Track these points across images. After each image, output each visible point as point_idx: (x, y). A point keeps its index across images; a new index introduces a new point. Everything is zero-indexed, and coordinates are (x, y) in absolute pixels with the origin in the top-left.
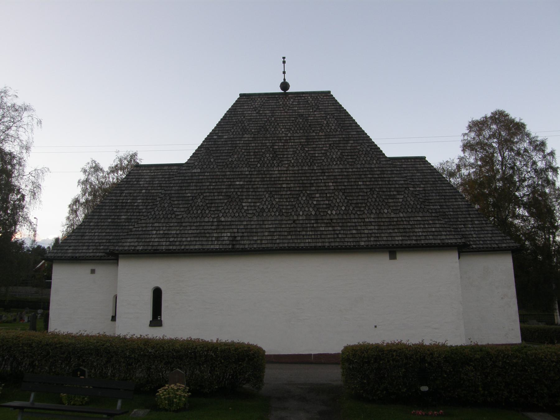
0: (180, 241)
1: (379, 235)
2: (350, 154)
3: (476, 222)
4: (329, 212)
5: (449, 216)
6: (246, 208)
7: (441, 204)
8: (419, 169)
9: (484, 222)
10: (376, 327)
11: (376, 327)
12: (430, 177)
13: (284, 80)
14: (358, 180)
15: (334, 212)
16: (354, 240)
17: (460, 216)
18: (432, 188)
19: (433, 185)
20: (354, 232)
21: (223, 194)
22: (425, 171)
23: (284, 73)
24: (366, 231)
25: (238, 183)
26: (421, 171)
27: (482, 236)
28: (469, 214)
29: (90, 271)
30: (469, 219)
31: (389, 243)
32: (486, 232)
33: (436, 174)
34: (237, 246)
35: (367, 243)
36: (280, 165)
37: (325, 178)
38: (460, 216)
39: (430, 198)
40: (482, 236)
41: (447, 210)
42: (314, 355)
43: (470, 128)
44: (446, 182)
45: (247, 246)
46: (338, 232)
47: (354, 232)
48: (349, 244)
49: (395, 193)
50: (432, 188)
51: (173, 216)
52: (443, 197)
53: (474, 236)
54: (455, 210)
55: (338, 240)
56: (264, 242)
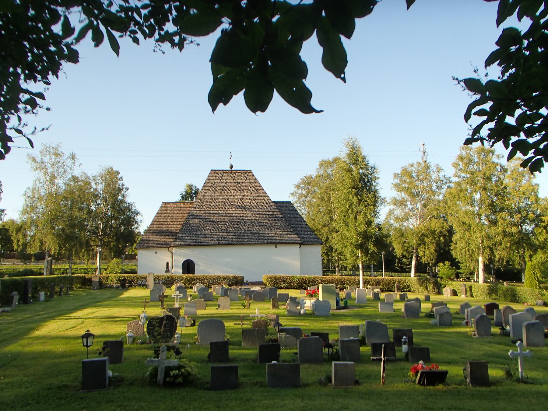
43: (321, 165)
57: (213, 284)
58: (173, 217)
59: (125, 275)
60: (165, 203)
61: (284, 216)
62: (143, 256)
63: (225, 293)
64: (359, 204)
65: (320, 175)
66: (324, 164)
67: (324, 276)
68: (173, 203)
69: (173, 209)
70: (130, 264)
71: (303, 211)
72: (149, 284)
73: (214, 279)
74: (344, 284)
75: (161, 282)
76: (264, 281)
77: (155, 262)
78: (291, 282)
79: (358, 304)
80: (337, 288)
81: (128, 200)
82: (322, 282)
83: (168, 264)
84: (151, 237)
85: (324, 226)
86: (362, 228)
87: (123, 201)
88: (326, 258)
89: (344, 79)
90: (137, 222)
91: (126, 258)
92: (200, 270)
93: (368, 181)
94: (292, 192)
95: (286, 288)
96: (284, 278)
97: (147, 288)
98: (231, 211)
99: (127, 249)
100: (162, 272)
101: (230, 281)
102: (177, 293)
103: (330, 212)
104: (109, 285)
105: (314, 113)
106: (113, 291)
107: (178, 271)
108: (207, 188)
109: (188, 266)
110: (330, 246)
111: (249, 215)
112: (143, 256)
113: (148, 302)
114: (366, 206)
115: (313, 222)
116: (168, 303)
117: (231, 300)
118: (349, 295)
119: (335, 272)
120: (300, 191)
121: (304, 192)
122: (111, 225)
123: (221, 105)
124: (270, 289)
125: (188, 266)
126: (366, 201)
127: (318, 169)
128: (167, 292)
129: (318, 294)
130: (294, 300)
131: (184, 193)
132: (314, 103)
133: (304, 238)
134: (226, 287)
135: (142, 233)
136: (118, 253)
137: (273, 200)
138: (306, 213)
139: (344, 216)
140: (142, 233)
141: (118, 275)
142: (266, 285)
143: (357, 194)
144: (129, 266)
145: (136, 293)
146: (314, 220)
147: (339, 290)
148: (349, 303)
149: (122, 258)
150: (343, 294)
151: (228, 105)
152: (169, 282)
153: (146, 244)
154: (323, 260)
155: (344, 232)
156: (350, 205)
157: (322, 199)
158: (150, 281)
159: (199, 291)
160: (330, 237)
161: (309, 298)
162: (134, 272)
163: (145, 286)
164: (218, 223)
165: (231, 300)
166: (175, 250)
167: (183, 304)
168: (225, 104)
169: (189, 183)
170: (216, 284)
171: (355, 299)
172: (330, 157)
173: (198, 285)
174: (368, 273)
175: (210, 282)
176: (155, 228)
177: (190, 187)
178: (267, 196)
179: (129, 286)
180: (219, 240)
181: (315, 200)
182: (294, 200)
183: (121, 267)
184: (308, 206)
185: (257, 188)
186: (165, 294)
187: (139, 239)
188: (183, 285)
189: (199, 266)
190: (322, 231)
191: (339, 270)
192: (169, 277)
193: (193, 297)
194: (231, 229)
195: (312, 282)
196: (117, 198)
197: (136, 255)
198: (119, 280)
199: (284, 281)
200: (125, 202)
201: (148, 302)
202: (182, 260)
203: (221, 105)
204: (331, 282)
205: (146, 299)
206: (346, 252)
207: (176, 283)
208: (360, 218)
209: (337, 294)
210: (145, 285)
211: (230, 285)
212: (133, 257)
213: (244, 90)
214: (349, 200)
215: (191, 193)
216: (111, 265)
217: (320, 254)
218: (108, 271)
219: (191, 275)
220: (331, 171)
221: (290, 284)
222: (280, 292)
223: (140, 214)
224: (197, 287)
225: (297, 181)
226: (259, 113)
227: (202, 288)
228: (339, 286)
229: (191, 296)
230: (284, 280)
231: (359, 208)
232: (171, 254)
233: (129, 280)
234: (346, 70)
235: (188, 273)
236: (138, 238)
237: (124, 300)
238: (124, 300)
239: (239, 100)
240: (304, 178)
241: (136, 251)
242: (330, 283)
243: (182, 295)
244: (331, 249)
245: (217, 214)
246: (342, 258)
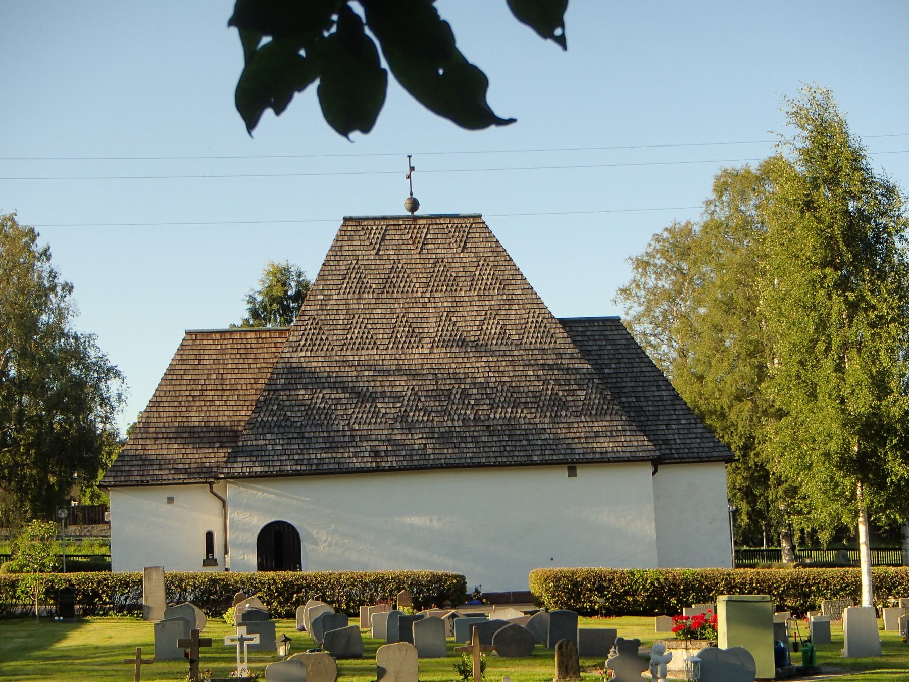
0: (308, 459)
1: (555, 447)
2: (515, 327)
3: (683, 422)
4: (492, 416)
5: (648, 413)
6: (383, 411)
7: (638, 394)
8: (610, 338)
9: (693, 421)
12: (625, 351)
13: (411, 194)
14: (526, 368)
16: (526, 453)
17: (662, 413)
18: (626, 370)
19: (628, 365)
20: (525, 442)
21: (350, 391)
22: (618, 342)
24: (540, 442)
26: (612, 342)
27: (688, 441)
28: (675, 410)
30: (674, 417)
31: (568, 457)
32: (693, 436)
33: (633, 346)
34: (383, 464)
35: (541, 458)
38: (662, 413)
39: (623, 385)
40: (688, 441)
41: (645, 404)
43: (721, 188)
44: (647, 360)
45: (395, 464)
46: (504, 443)
47: (525, 442)
48: (519, 459)
49: (575, 387)
50: (626, 370)
51: (289, 423)
52: (641, 384)
53: (678, 441)
54: (656, 403)
55: (506, 454)
57: (362, 603)
58: (222, 381)
59: (72, 575)
60: (194, 336)
61: (599, 368)
62: (123, 507)
63: (402, 630)
64: (851, 318)
65: (719, 225)
66: (732, 184)
67: (742, 570)
68: (222, 333)
69: (222, 352)
70: (86, 541)
71: (663, 351)
72: (150, 604)
73: (366, 584)
74: (807, 595)
75: (190, 597)
76: (535, 588)
77: (166, 532)
78: (626, 593)
79: (851, 660)
80: (780, 609)
81: (75, 325)
82: (730, 588)
83: (209, 536)
84: (152, 451)
85: (738, 398)
86: (861, 403)
87: (55, 331)
88: (745, 507)
89: (562, 41)
90: (104, 401)
91: (73, 519)
92: (320, 557)
93: (877, 237)
94: (626, 282)
95: (609, 613)
96: (600, 577)
97: (145, 619)
98: (415, 357)
99: (76, 491)
100: (189, 563)
101: (420, 591)
102: (242, 631)
103: (756, 350)
104: (19, 610)
105: (493, 128)
106: (31, 627)
107: (243, 560)
108: (334, 280)
109: (279, 545)
110: (761, 467)
111: (477, 368)
112: (123, 507)
113: (148, 662)
114: (872, 325)
115: (697, 386)
116: (210, 665)
117: (420, 656)
118: (821, 629)
119: (776, 555)
120: (651, 281)
121: (665, 283)
122: (21, 413)
123: (269, 113)
124: (553, 615)
125: (279, 545)
126: (874, 308)
127: (709, 203)
128: (210, 629)
129: (715, 629)
130: (630, 648)
131: (259, 298)
132: (497, 100)
133: (666, 442)
134: (406, 610)
135: (123, 435)
136: (48, 504)
137: (558, 315)
138: (674, 354)
139: (801, 363)
140: (123, 435)
141: (49, 576)
142: (540, 604)
143: (843, 285)
144: (85, 547)
145: (110, 633)
146: (701, 378)
147: (788, 614)
148: (822, 655)
149: (59, 520)
150: (801, 630)
151: (284, 114)
152: (216, 597)
153: (139, 471)
154: (735, 514)
155: (802, 418)
156: (822, 325)
157: (729, 306)
158: (154, 596)
159: (315, 624)
160: (758, 434)
161: (683, 644)
162: (100, 564)
163: (135, 610)
164: (373, 398)
165: (420, 656)
166: (232, 491)
167: (263, 669)
168: (278, 112)
169: (281, 261)
170: (372, 602)
171: (840, 644)
172: (751, 158)
173: (311, 604)
174: (892, 556)
175: (349, 596)
176: (165, 416)
177: (281, 275)
178: (538, 302)
179: (86, 613)
180: (377, 453)
181: (702, 311)
182: (632, 312)
183: (56, 549)
184: (678, 331)
185: (502, 275)
186: (203, 635)
187: (114, 457)
188: (264, 607)
189: (315, 542)
190: (732, 417)
191: (793, 548)
192: (214, 581)
193: (295, 646)
194: (421, 417)
195: (698, 590)
196: (35, 320)
197: (104, 508)
198: (48, 592)
199: (601, 590)
200: (63, 334)
201: (148, 662)
202: (260, 522)
203: (269, 113)
204: (764, 587)
205: (139, 652)
206: (812, 487)
207: (239, 600)
208: (854, 364)
209: (780, 629)
210: (140, 607)
211: (418, 606)
212: (95, 516)
213: (317, 82)
214: (814, 307)
215: (280, 300)
216: (23, 542)
217: (725, 493)
218: (14, 564)
219: (289, 575)
220: (757, 207)
221: (623, 598)
222: (583, 623)
223: (117, 375)
224: (311, 610)
225: (641, 246)
226: (356, 135)
227: (326, 616)
228: (790, 602)
229: (286, 639)
230: (601, 583)
231: (851, 334)
232: (219, 504)
233: (84, 593)
234: (568, 17)
235: (279, 566)
236: (110, 454)
237: (69, 657)
238: (66, 656)
239: (307, 102)
240: (666, 235)
241: (103, 494)
242: (760, 591)
243: (256, 639)
244: (760, 477)
245: (370, 367)
246: (799, 505)
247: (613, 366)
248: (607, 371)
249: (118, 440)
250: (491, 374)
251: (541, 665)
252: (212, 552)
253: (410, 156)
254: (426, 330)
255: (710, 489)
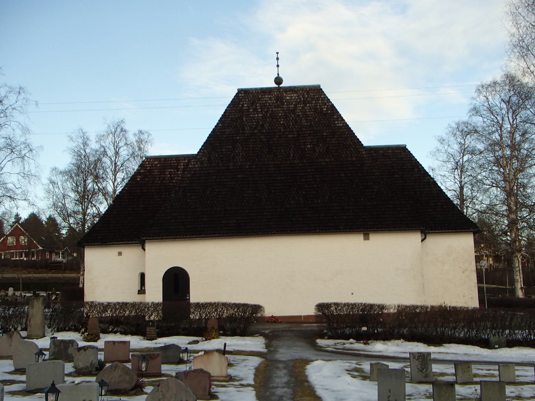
10: (352, 294)
11: (352, 294)
13: (278, 74)
15: (320, 201)
23: (278, 66)
24: (345, 217)
25: (240, 176)
29: (117, 254)
36: (275, 159)
37: (313, 170)
42: (304, 316)
49: (372, 184)
56: (262, 227)
247: (400, 173)
248: (396, 176)
249: (259, 315)
250: (309, 170)
251: (289, 347)
252: (144, 286)
253: (277, 53)
254: (279, 151)
255: (460, 247)
